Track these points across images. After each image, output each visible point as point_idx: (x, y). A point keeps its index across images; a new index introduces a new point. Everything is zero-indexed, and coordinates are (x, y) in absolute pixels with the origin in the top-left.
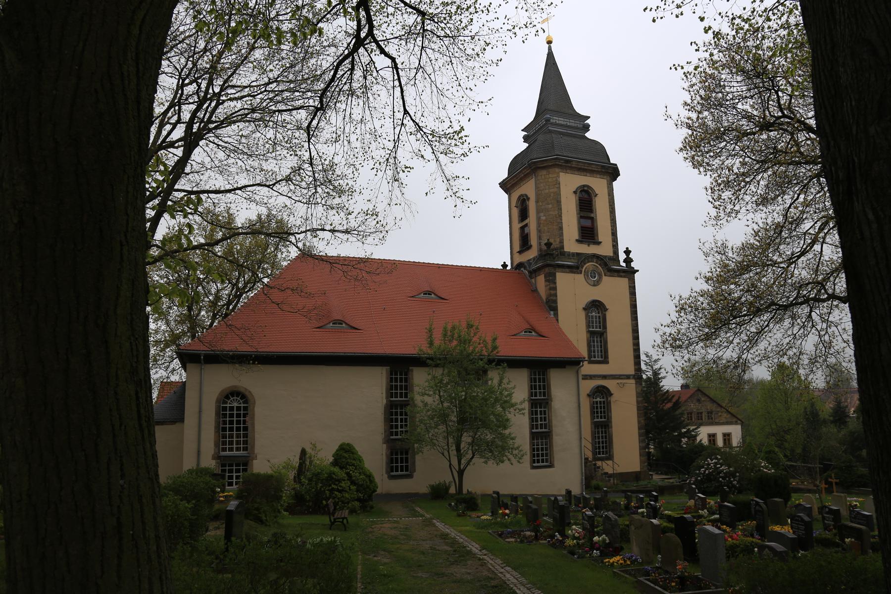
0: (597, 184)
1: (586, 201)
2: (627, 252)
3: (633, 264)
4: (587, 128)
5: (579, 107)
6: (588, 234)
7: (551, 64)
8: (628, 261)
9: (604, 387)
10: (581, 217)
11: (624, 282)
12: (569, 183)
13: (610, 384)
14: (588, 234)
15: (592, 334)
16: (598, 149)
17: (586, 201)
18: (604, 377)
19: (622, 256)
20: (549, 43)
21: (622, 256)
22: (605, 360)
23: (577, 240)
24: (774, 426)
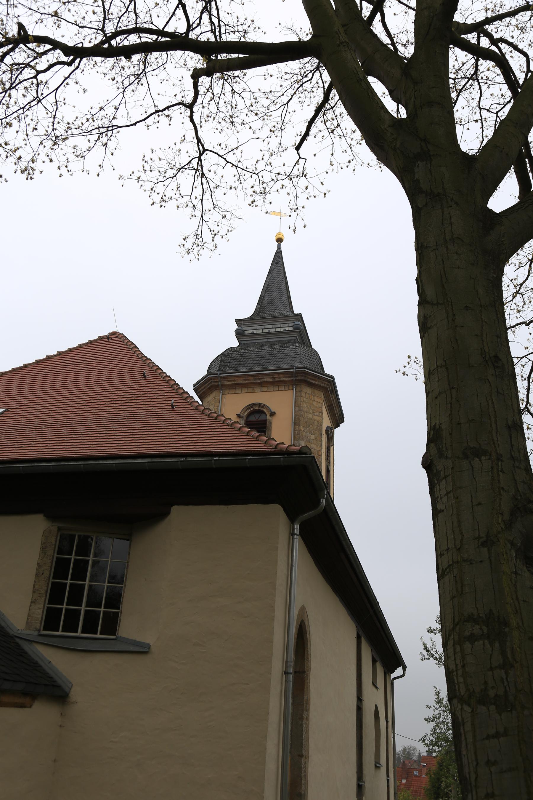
20: (280, 240)
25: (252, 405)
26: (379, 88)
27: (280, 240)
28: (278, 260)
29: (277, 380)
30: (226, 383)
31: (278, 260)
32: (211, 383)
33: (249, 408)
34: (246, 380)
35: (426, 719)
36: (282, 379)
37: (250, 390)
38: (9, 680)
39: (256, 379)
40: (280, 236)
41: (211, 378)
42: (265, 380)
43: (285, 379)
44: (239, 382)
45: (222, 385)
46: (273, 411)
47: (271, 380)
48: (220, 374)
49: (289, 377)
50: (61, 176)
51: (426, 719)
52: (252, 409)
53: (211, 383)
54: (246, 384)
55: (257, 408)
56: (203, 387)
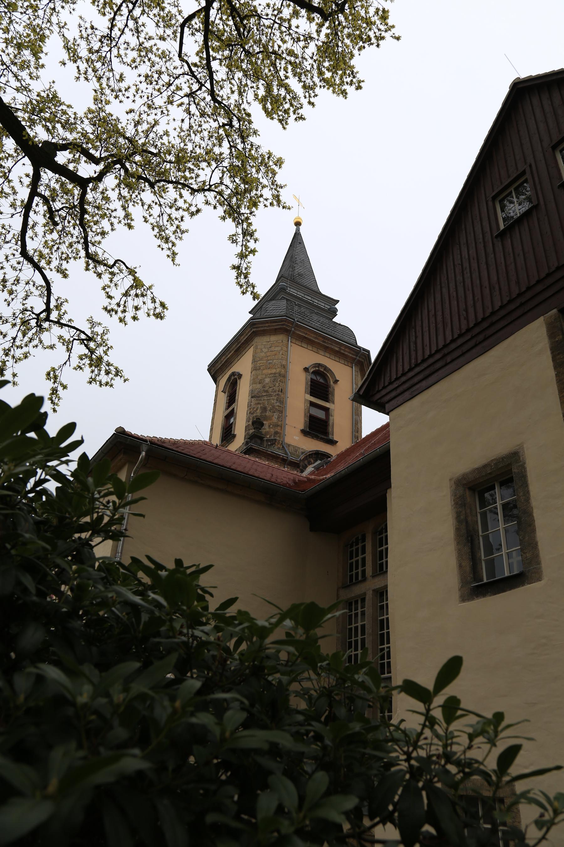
4: (334, 313)
20: (298, 224)
25: (319, 365)
26: (353, 663)
27: (298, 224)
28: (297, 240)
29: (342, 351)
30: (297, 332)
31: (297, 240)
32: (283, 325)
33: (315, 367)
34: (316, 338)
35: (304, 119)
36: (346, 353)
37: (315, 349)
38: (232, 399)
39: (325, 342)
40: (299, 220)
41: (286, 320)
42: (333, 347)
43: (349, 354)
44: (309, 337)
45: (294, 332)
46: (337, 379)
47: (337, 349)
48: (298, 321)
49: (352, 354)
50: (121, 102)
51: (304, 119)
52: (317, 369)
53: (283, 325)
54: (314, 342)
55: (322, 370)
56: (267, 325)
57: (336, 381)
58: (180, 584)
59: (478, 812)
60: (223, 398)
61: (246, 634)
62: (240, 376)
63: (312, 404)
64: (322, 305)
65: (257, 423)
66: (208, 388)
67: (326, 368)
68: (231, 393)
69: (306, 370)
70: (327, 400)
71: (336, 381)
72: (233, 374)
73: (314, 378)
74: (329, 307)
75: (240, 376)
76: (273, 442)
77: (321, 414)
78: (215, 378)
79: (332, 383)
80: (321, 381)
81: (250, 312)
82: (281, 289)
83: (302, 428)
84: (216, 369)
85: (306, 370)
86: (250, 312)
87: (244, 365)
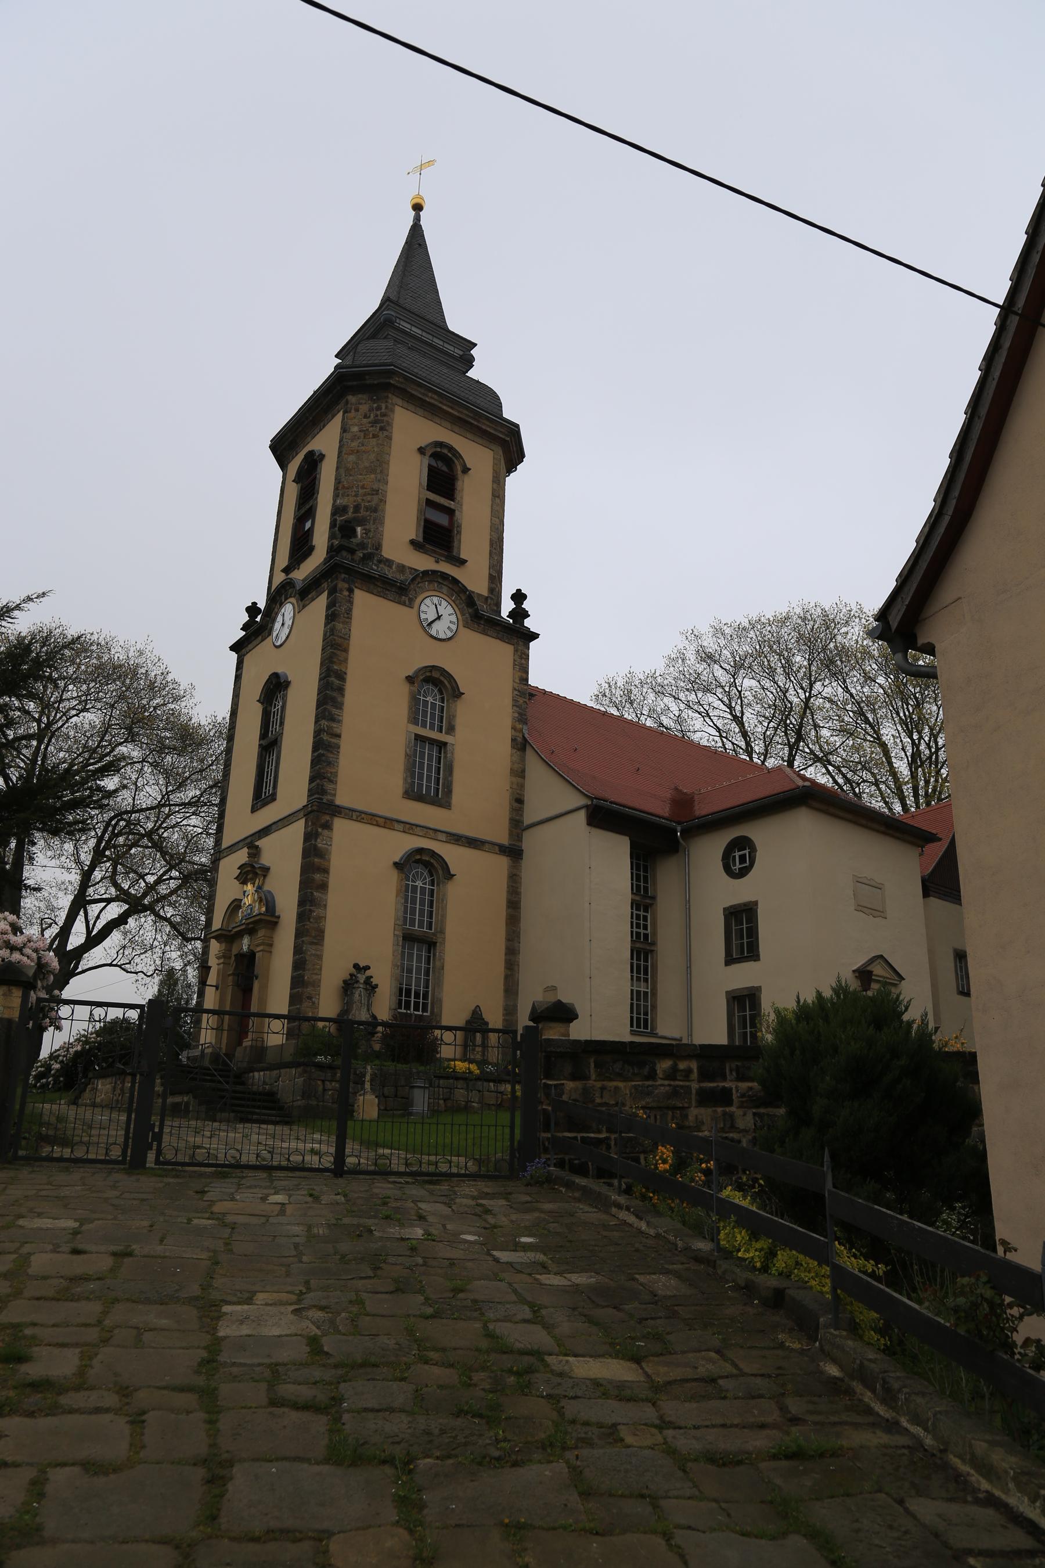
0: (476, 456)
1: (443, 475)
2: (519, 597)
3: (527, 622)
4: (469, 362)
5: (456, 322)
6: (438, 536)
7: (416, 243)
8: (519, 614)
9: (433, 854)
10: (429, 503)
11: (503, 651)
12: (411, 432)
13: (452, 855)
14: (438, 536)
15: (409, 938)
16: (487, 401)
17: (443, 475)
18: (432, 832)
19: (507, 606)
20: (418, 208)
21: (507, 606)
22: (441, 798)
23: (413, 542)
24: (362, 929)
25: (440, 444)
27: (418, 208)
31: (416, 243)
56: (255, 1117)
57: (466, 470)
58: (700, 1250)
59: (860, 1198)
60: (293, 489)
61: (8, 867)
62: (322, 457)
63: (429, 503)
64: (450, 349)
65: (343, 528)
66: (269, 477)
67: (451, 449)
68: (305, 482)
69: (421, 451)
70: (452, 498)
71: (466, 470)
72: (311, 453)
73: (434, 464)
74: (461, 353)
75: (322, 457)
76: (368, 557)
77: (442, 520)
78: (283, 463)
79: (459, 472)
80: (445, 469)
81: (336, 356)
82: (385, 320)
83: (413, 536)
84: (283, 446)
85: (421, 451)
86: (336, 356)
87: (326, 441)
